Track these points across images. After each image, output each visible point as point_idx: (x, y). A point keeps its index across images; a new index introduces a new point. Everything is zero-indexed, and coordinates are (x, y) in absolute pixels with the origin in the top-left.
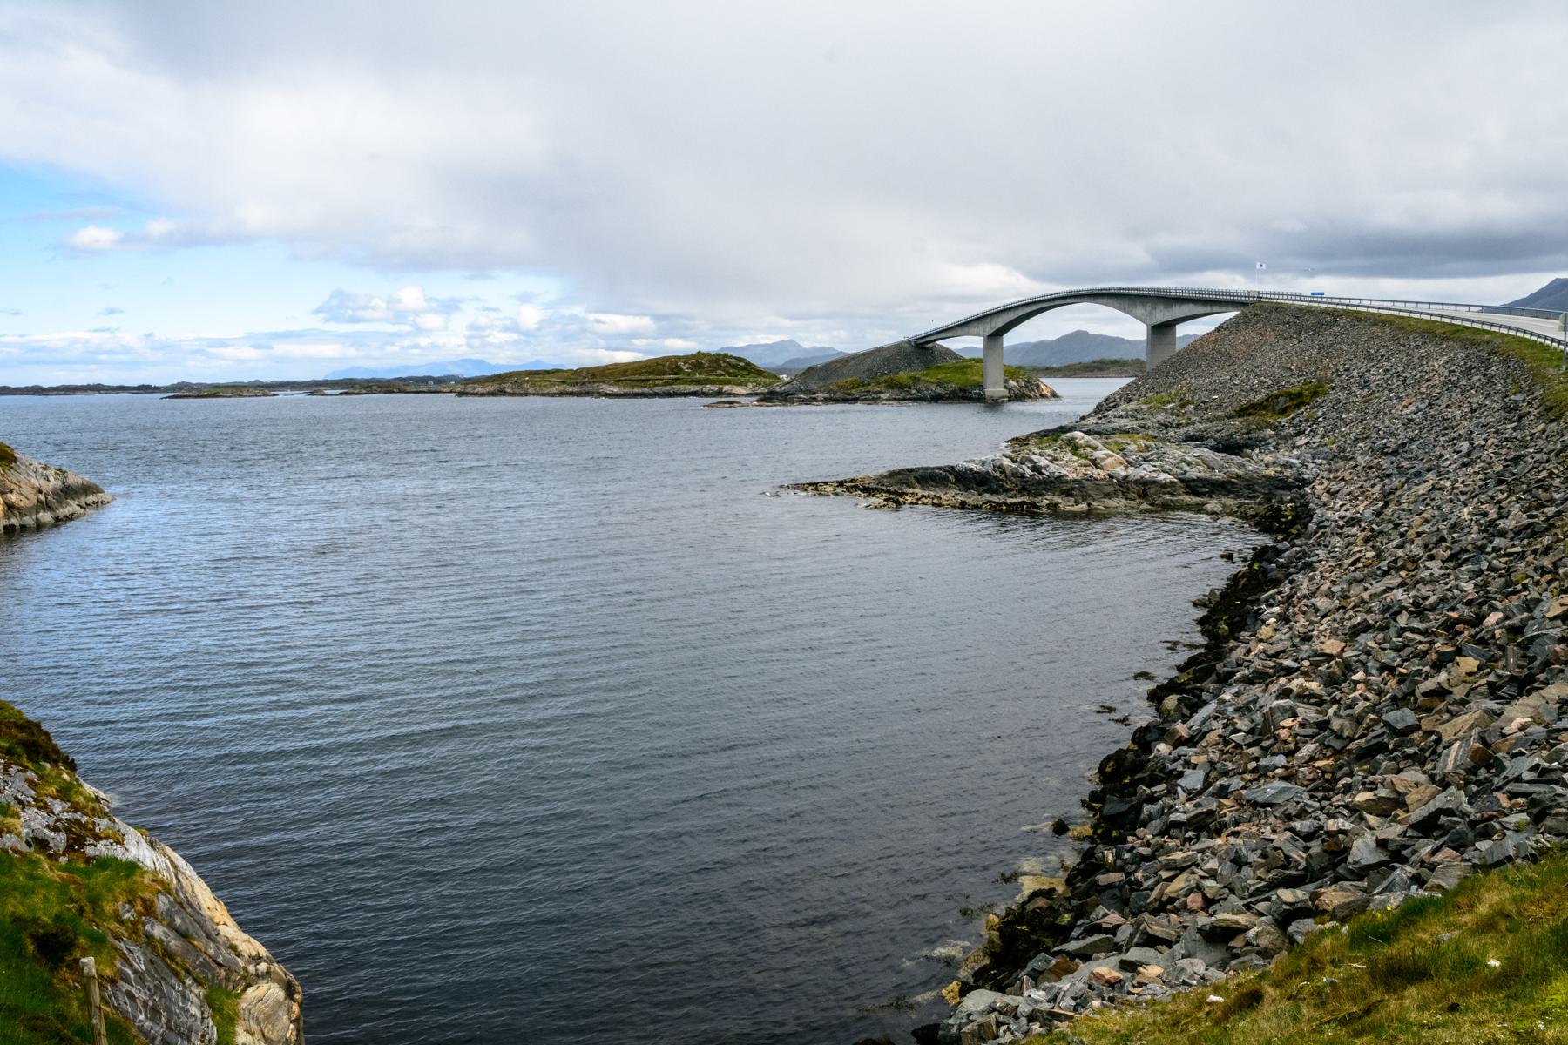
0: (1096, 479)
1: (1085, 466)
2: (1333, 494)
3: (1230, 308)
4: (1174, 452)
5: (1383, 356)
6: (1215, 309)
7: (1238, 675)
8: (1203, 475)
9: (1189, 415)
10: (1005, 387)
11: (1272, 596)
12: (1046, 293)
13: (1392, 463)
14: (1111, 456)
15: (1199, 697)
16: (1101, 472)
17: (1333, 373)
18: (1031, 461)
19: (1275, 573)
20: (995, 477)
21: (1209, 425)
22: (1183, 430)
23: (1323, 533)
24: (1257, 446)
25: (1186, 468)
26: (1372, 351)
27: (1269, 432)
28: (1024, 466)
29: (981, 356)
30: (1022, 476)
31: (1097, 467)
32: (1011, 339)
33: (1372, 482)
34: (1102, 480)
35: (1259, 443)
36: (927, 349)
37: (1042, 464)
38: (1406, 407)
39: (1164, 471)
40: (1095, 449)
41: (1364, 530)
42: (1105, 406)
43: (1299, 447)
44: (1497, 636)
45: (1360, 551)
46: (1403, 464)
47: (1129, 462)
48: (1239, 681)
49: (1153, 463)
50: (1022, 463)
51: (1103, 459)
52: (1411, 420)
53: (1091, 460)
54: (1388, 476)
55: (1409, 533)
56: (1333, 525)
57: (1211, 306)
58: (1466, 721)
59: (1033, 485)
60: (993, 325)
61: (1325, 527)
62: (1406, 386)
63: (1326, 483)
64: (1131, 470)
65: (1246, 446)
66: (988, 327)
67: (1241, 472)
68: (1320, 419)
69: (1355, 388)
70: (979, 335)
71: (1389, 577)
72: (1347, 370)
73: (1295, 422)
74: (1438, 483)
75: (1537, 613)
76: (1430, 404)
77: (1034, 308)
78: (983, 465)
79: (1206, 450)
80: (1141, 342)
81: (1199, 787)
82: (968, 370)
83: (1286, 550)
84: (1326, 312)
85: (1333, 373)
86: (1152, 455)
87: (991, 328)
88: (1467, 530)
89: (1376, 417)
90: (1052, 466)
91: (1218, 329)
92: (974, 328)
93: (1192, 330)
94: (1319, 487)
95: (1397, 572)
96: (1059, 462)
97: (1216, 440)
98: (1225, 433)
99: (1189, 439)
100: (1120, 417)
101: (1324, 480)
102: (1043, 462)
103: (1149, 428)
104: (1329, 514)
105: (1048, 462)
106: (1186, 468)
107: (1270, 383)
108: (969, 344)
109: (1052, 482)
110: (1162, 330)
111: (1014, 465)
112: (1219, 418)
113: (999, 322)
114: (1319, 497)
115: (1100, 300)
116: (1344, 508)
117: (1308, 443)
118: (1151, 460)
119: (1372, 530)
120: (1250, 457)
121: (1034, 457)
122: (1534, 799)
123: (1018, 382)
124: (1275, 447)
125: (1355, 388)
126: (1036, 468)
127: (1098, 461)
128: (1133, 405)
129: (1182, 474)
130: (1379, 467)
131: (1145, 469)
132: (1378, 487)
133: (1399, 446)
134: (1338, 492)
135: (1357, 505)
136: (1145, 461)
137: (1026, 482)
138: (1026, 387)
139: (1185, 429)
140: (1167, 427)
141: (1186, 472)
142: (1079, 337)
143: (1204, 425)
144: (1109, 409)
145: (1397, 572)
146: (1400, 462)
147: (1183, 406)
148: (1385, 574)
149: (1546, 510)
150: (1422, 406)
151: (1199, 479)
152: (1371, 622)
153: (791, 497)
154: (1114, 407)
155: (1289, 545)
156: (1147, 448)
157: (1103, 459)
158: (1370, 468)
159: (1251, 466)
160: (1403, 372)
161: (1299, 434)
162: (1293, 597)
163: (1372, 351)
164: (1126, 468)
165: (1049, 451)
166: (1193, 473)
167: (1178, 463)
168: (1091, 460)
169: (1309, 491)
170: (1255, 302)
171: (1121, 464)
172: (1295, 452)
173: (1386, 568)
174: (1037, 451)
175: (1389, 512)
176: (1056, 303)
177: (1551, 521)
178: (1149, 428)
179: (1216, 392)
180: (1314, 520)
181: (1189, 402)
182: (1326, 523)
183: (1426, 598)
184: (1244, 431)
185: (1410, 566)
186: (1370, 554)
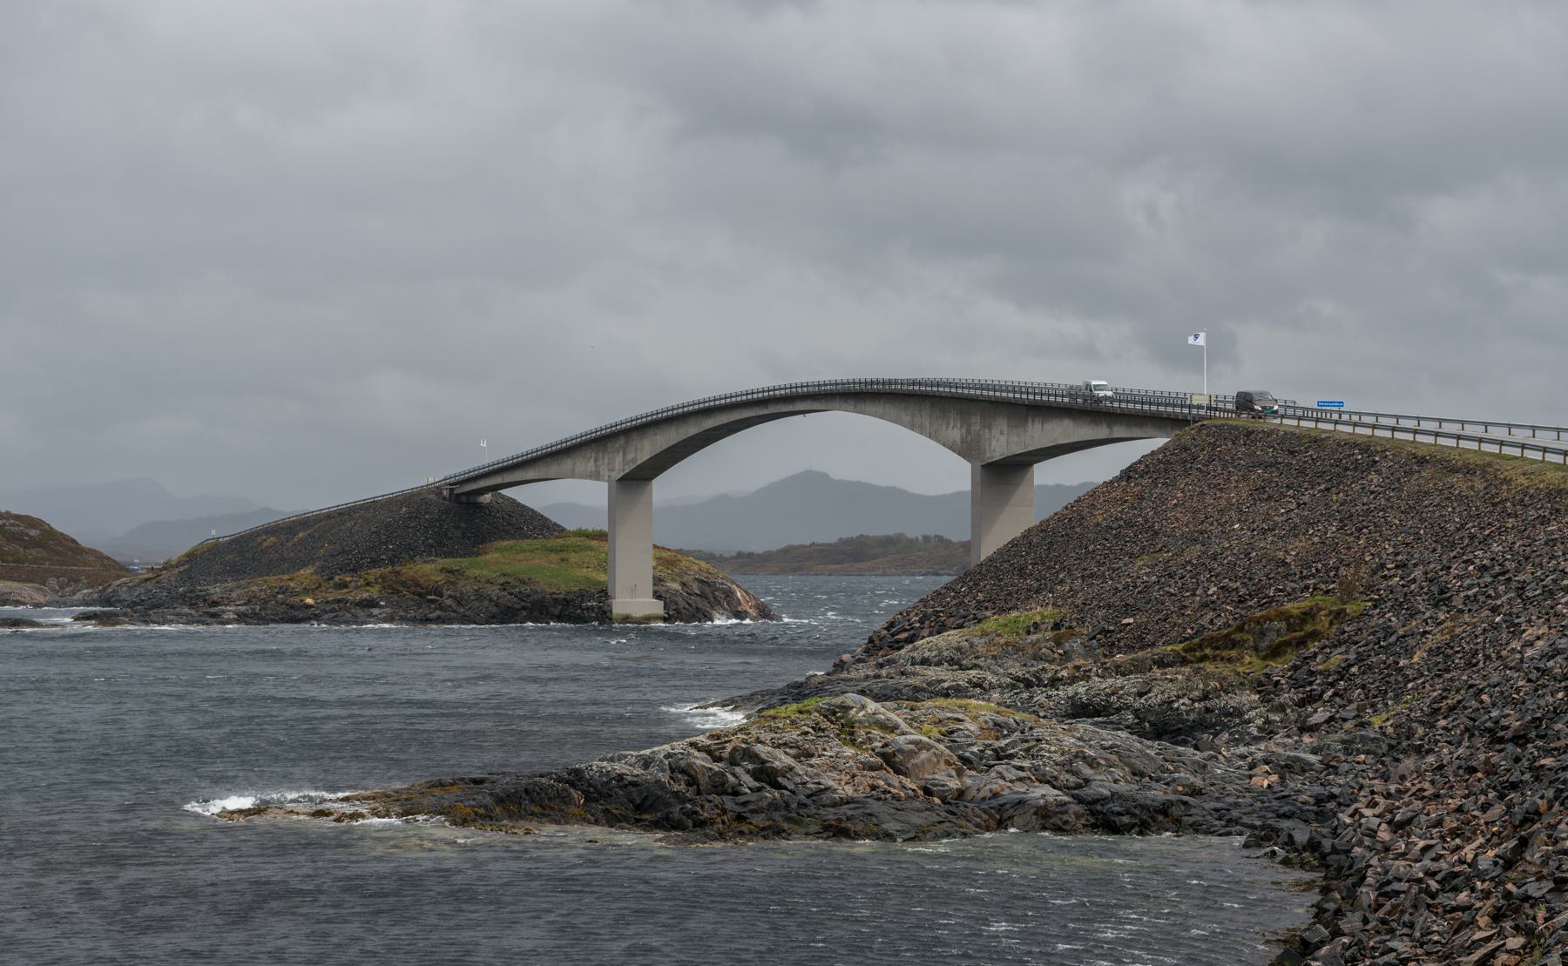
0: (897, 798)
1: (872, 768)
3: (1149, 430)
6: (1119, 431)
8: (1122, 787)
10: (657, 596)
12: (728, 392)
13: (1517, 760)
14: (928, 747)
17: (1374, 572)
18: (752, 756)
20: (676, 794)
21: (1120, 681)
22: (1064, 692)
23: (1394, 907)
24: (1226, 727)
25: (1087, 771)
26: (1451, 527)
28: (738, 770)
29: (603, 526)
31: (898, 772)
32: (664, 488)
33: (1482, 798)
34: (908, 798)
36: (479, 506)
37: (777, 764)
39: (1043, 780)
40: (893, 728)
41: (1487, 895)
43: (1312, 729)
45: (1488, 939)
49: (1016, 762)
50: (733, 762)
51: (912, 754)
54: (1514, 786)
56: (1415, 889)
57: (1129, 425)
60: (630, 456)
61: (1397, 893)
62: (1527, 601)
64: (970, 779)
65: (1202, 725)
66: (619, 459)
68: (1354, 670)
70: (596, 476)
77: (723, 419)
78: (646, 765)
79: (1124, 734)
80: (958, 495)
82: (574, 557)
83: (1322, 943)
84: (1352, 444)
85: (1374, 572)
86: (1013, 744)
87: (625, 462)
89: (1470, 665)
90: (799, 769)
91: (1128, 474)
92: (585, 462)
94: (1368, 812)
96: (813, 761)
97: (1136, 712)
99: (1080, 710)
100: (925, 662)
101: (1377, 798)
103: (992, 686)
105: (790, 761)
106: (1087, 771)
107: (1243, 591)
111: (716, 767)
113: (645, 449)
114: (1372, 834)
115: (869, 407)
117: (1332, 719)
118: (1011, 757)
119: (1508, 895)
127: (900, 757)
128: (952, 637)
129: (1078, 786)
130: (1491, 769)
132: (1498, 809)
133: (1526, 727)
134: (1409, 821)
135: (1458, 848)
136: (999, 758)
137: (745, 804)
138: (703, 595)
139: (1070, 690)
141: (1087, 781)
142: (811, 484)
143: (1110, 681)
144: (897, 646)
146: (1535, 759)
154: (910, 640)
155: (1326, 932)
157: (912, 754)
158: (1472, 770)
161: (1311, 699)
163: (1451, 527)
164: (960, 773)
166: (1102, 784)
170: (1203, 418)
175: (1535, 855)
176: (772, 409)
178: (992, 686)
179: (1128, 609)
180: (1370, 880)
182: (1396, 886)
186: (1515, 942)
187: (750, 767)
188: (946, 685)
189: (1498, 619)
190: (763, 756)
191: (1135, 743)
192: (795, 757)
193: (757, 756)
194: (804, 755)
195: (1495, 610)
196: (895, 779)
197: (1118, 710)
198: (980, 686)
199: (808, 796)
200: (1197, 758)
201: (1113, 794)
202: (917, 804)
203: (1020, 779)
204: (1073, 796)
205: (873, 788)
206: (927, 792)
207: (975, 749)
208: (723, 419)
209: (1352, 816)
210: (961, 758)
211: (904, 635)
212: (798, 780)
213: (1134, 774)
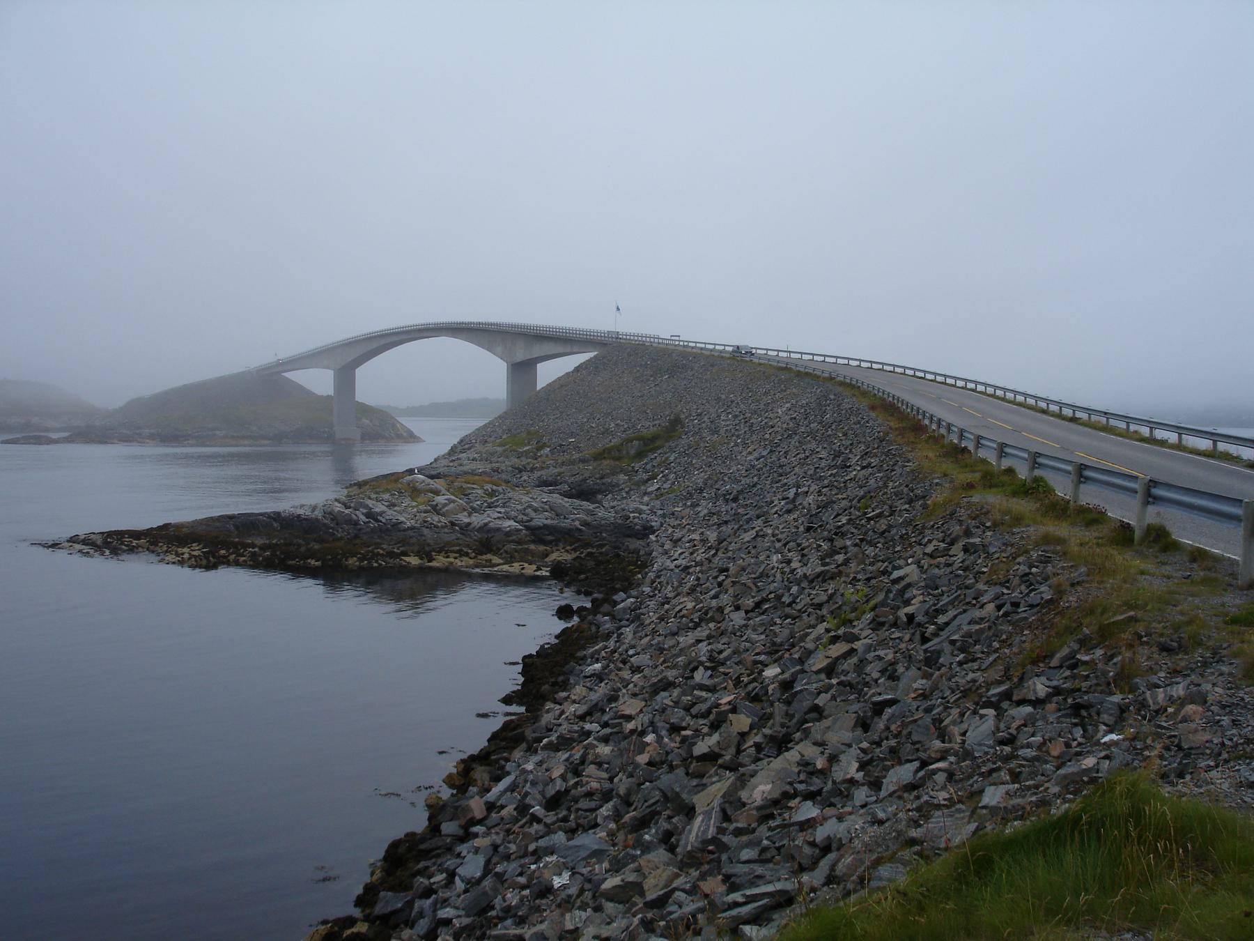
1: (426, 512)
2: (676, 542)
4: (521, 498)
5: (732, 402)
7: (545, 741)
8: (548, 522)
9: (544, 458)
11: (598, 652)
14: (454, 501)
15: (503, 768)
16: (443, 519)
18: (367, 507)
19: (607, 626)
20: (325, 525)
25: (533, 514)
27: (622, 477)
30: (356, 523)
31: (438, 514)
34: (442, 527)
35: (611, 489)
37: (377, 510)
38: (750, 453)
42: (460, 448)
44: (770, 692)
46: (739, 511)
47: (473, 509)
48: (545, 748)
49: (498, 509)
52: (753, 466)
53: (431, 506)
55: (726, 583)
58: (719, 789)
59: (365, 533)
63: (670, 530)
65: (600, 492)
67: (589, 519)
69: (705, 433)
70: (328, 368)
71: (699, 629)
72: (700, 415)
73: (649, 467)
74: (762, 530)
75: (806, 667)
76: (771, 451)
81: (478, 874)
86: (497, 501)
88: (771, 578)
90: (390, 512)
91: (577, 369)
93: (549, 372)
95: (707, 625)
98: (578, 478)
99: (543, 483)
102: (379, 508)
104: (668, 563)
105: (384, 508)
106: (533, 514)
108: (320, 381)
109: (388, 530)
110: (522, 370)
111: (347, 511)
112: (572, 463)
116: (683, 556)
118: (496, 507)
120: (600, 503)
121: (370, 503)
122: (733, 882)
123: (371, 421)
124: (627, 493)
125: (705, 433)
126: (370, 515)
131: (488, 516)
134: (680, 539)
137: (360, 529)
140: (520, 471)
145: (707, 625)
147: (539, 449)
148: (697, 625)
149: (836, 557)
150: (765, 453)
151: (545, 526)
152: (671, 679)
153: (35, 547)
154: (469, 449)
156: (492, 494)
159: (601, 513)
160: (750, 418)
162: (615, 652)
165: (386, 496)
166: (540, 520)
167: (525, 509)
168: (431, 506)
169: (654, 539)
171: (464, 510)
172: (646, 499)
173: (697, 620)
174: (373, 496)
177: (840, 568)
179: (572, 435)
181: (544, 446)
183: (721, 652)
184: (598, 476)
185: (718, 616)
187: (365, 511)
188: (480, 471)
189: (739, 441)
190: (371, 506)
191: (566, 502)
192: (387, 506)
193: (368, 506)
194: (391, 505)
195: (738, 437)
196: (436, 518)
197: (561, 483)
198: (497, 471)
199: (392, 526)
200: (591, 508)
201: (544, 525)
202: (446, 530)
203: (499, 518)
204: (525, 526)
205: (425, 522)
206: (453, 524)
207: (478, 503)
208: (400, 338)
209: (657, 536)
210: (471, 507)
211: (467, 446)
212: (388, 517)
213: (557, 515)
